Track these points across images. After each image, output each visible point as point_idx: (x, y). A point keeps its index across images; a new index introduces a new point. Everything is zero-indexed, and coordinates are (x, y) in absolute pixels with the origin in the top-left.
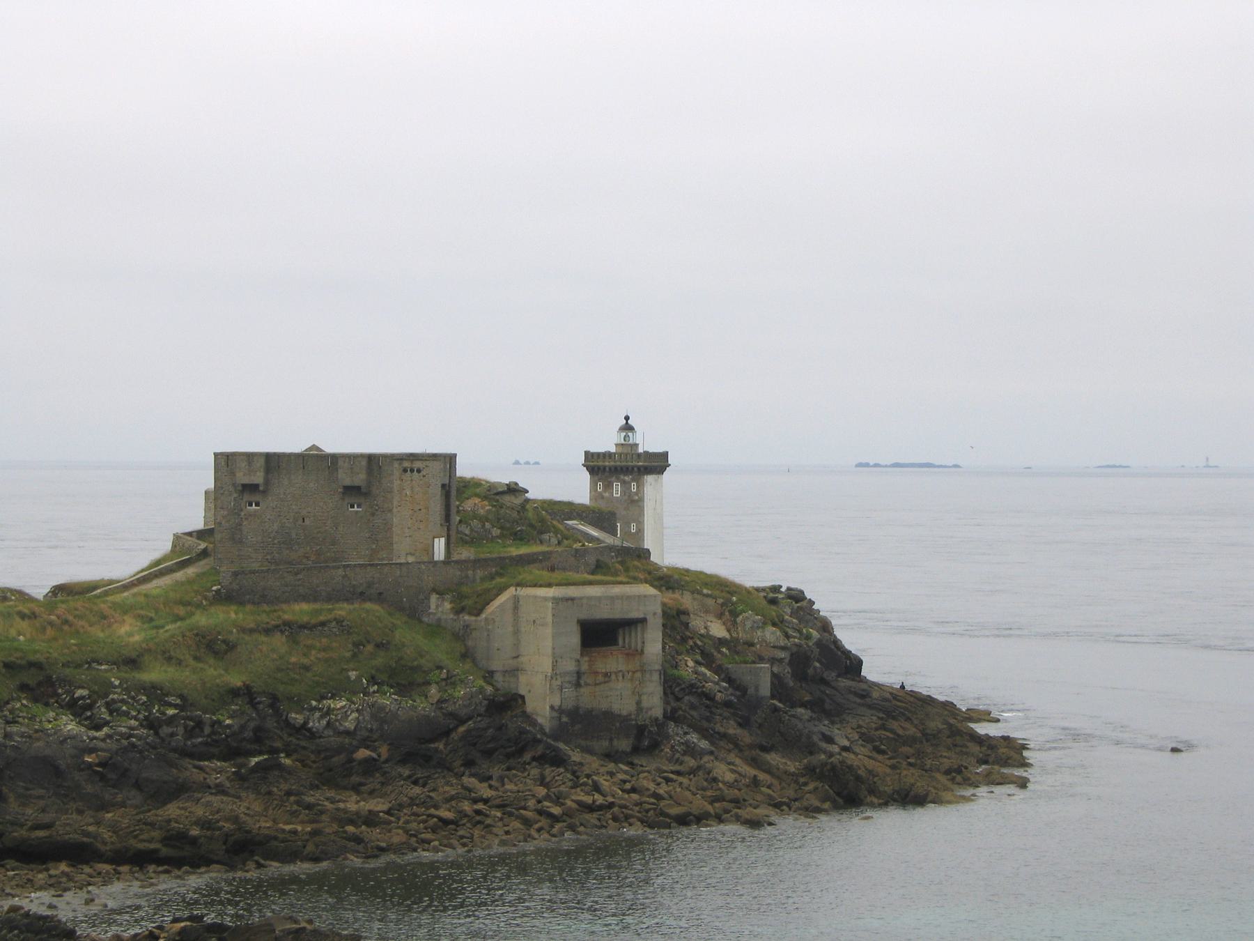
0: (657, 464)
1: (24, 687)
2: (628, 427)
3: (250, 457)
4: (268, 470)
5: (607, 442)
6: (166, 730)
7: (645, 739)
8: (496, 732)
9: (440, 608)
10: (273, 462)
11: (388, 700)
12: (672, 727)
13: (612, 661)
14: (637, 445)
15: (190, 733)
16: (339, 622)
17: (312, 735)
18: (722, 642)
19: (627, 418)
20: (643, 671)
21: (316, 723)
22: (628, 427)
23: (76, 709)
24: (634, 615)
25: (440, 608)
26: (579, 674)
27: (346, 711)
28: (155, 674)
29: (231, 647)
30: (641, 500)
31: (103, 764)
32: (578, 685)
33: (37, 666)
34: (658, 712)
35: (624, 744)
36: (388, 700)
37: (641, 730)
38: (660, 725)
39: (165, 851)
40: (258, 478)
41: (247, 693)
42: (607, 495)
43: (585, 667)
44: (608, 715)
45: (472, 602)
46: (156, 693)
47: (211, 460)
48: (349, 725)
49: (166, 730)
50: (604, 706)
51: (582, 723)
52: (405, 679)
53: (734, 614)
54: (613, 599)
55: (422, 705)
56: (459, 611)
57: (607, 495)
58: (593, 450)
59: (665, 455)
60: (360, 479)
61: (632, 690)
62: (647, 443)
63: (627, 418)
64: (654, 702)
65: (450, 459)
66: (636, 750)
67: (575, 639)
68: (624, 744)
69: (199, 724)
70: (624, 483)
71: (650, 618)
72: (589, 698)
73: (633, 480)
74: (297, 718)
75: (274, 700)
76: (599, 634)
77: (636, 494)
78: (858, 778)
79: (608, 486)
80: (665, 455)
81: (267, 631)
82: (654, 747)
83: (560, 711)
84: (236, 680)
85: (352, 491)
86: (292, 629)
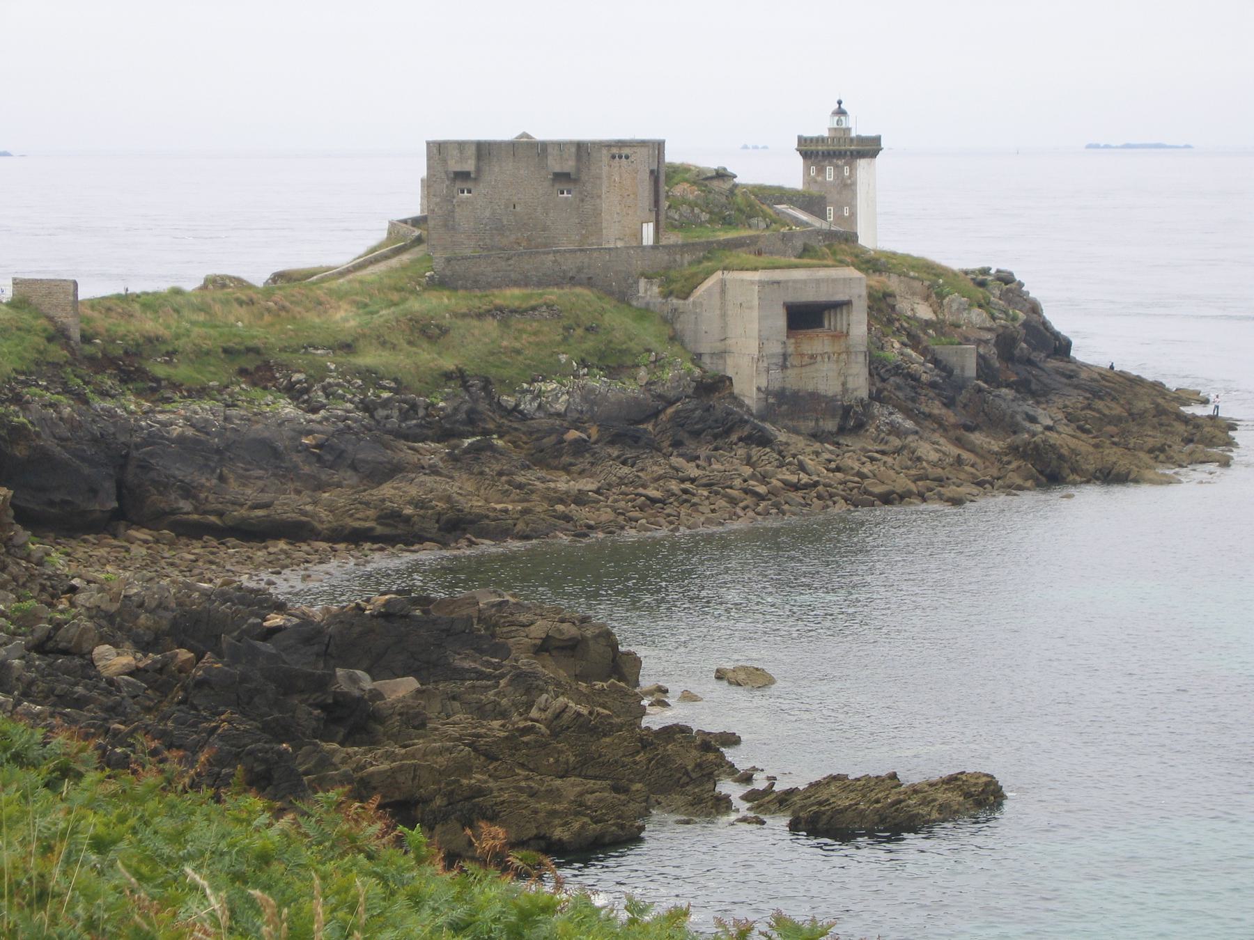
0: (869, 148)
3: (461, 145)
4: (579, 157)
5: (820, 127)
6: (381, 413)
7: (851, 420)
9: (648, 292)
11: (598, 383)
12: (877, 408)
13: (817, 343)
14: (849, 129)
15: (405, 416)
17: (524, 417)
18: (928, 324)
19: (840, 103)
20: (848, 352)
21: (528, 405)
22: (840, 112)
25: (648, 292)
26: (785, 356)
27: (558, 394)
28: (370, 358)
29: (444, 331)
30: (854, 184)
32: (784, 367)
33: (249, 350)
34: (863, 393)
35: (830, 425)
37: (847, 411)
39: (380, 530)
40: (470, 166)
41: (459, 377)
42: (819, 179)
43: (791, 349)
44: (814, 396)
45: (680, 286)
46: (371, 377)
48: (560, 407)
49: (381, 413)
50: (810, 388)
51: (788, 404)
52: (614, 362)
54: (818, 282)
55: (631, 388)
56: (667, 295)
57: (819, 179)
61: (838, 372)
62: (860, 127)
63: (840, 103)
64: (860, 384)
65: (659, 146)
66: (842, 430)
67: (781, 322)
69: (414, 407)
70: (836, 167)
71: (856, 302)
72: (795, 380)
73: (846, 164)
74: (509, 401)
75: (487, 383)
76: (804, 317)
77: (850, 177)
78: (1061, 457)
79: (821, 171)
82: (860, 426)
83: (768, 392)
84: (449, 364)
85: (562, 178)
86: (503, 314)
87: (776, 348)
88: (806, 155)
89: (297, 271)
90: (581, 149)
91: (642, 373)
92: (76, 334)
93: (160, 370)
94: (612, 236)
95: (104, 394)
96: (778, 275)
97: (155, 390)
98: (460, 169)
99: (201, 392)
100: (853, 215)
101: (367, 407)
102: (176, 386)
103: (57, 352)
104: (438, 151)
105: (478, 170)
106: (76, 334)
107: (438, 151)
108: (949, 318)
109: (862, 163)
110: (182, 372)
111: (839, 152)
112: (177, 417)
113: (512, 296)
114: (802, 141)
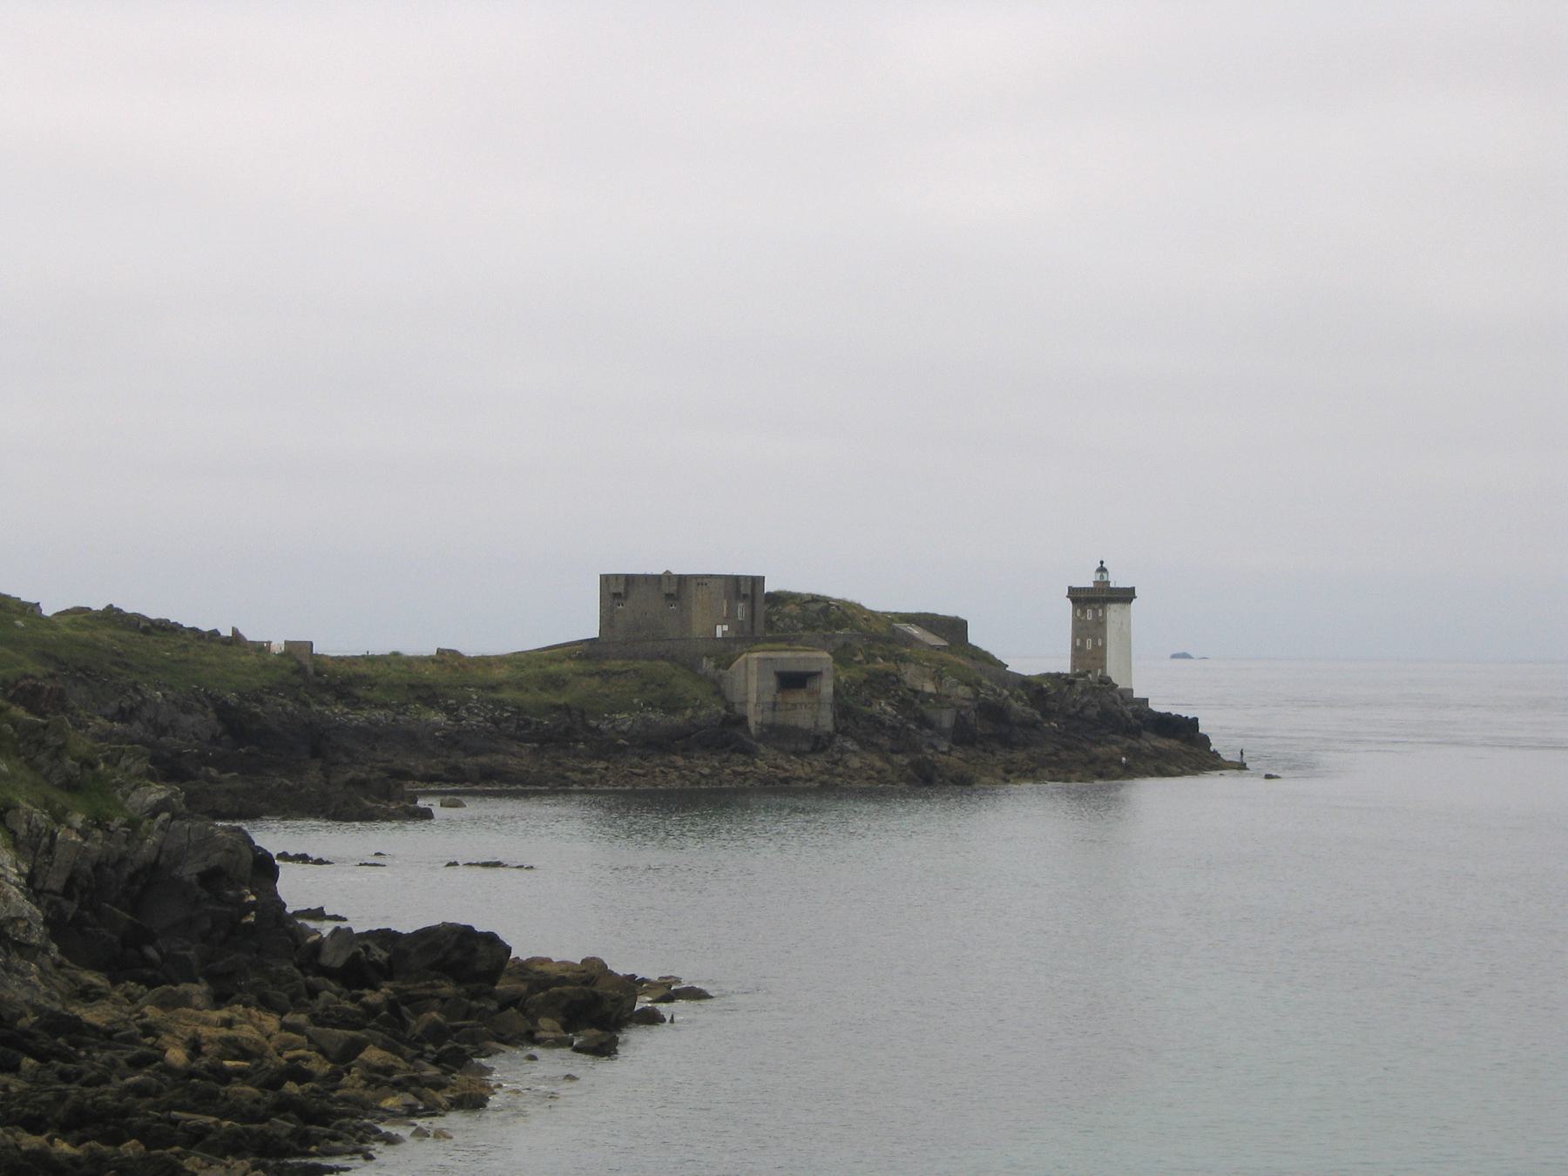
0: (1126, 596)
1: (419, 698)
2: (1102, 570)
3: (617, 576)
4: (679, 584)
5: (1087, 580)
6: (503, 725)
7: (819, 743)
8: (727, 735)
9: (708, 665)
10: (630, 580)
11: (655, 716)
12: (839, 739)
13: (799, 697)
15: (519, 727)
16: (635, 671)
17: (601, 733)
18: (931, 695)
20: (819, 703)
21: (604, 726)
22: (1102, 570)
23: (448, 710)
24: (814, 669)
25: (708, 665)
26: (775, 704)
27: (625, 720)
28: (506, 695)
29: (565, 683)
31: (444, 737)
32: (774, 709)
33: (426, 686)
34: (830, 728)
35: (806, 747)
36: (655, 716)
37: (817, 738)
38: (831, 737)
39: (446, 775)
40: (621, 589)
41: (566, 709)
43: (779, 699)
44: (795, 728)
45: (725, 662)
46: (500, 705)
47: (962, 616)
48: (624, 728)
49: (503, 725)
50: (792, 722)
51: (778, 734)
52: (671, 705)
53: (941, 678)
54: (798, 660)
55: (678, 720)
56: (717, 667)
58: (1076, 585)
59: (1133, 589)
60: (673, 589)
61: (813, 713)
62: (1117, 580)
64: (826, 721)
66: (813, 751)
67: (773, 683)
68: (806, 747)
69: (528, 723)
71: (825, 674)
72: (780, 718)
74: (593, 723)
75: (583, 713)
76: (792, 681)
78: (934, 767)
79: (1084, 612)
80: (1133, 589)
81: (591, 675)
82: (824, 748)
83: (762, 724)
84: (561, 701)
85: (669, 596)
86: (606, 675)
87: (768, 698)
88: (1074, 601)
89: (349, 625)
90: (682, 579)
91: (689, 712)
92: (311, 670)
93: (360, 692)
94: (698, 630)
95: (322, 703)
96: (771, 655)
97: (356, 703)
98: (619, 591)
99: (384, 706)
100: (1104, 645)
101: (496, 722)
102: (368, 702)
103: (297, 680)
104: (605, 579)
105: (627, 592)
106: (311, 670)
107: (605, 579)
108: (944, 691)
109: (1113, 612)
110: (376, 694)
111: (1097, 601)
112: (360, 717)
113: (615, 665)
114: (1070, 589)
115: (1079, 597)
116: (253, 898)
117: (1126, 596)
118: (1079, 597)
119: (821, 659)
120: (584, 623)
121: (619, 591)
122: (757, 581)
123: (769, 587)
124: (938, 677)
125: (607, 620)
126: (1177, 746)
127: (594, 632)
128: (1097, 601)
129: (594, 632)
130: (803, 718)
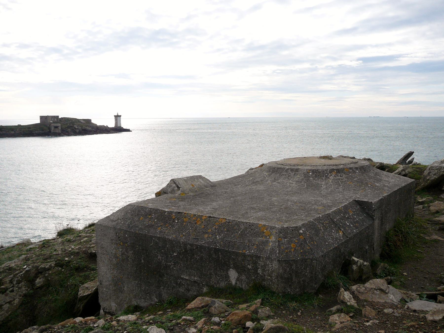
13: (56, 129)
41: (30, 131)
55: (43, 132)
64: (60, 132)
76: (56, 127)
98: (42, 118)
109: (118, 118)
111: (117, 117)
115: (115, 116)
116: (283, 312)
117: (120, 116)
118: (115, 116)
119: (59, 125)
120: (38, 121)
121: (42, 118)
122: (58, 116)
123: (60, 117)
124: (78, 126)
125: (41, 121)
126: (413, 152)
127: (39, 122)
128: (117, 117)
129: (39, 122)
130: (57, 131)
